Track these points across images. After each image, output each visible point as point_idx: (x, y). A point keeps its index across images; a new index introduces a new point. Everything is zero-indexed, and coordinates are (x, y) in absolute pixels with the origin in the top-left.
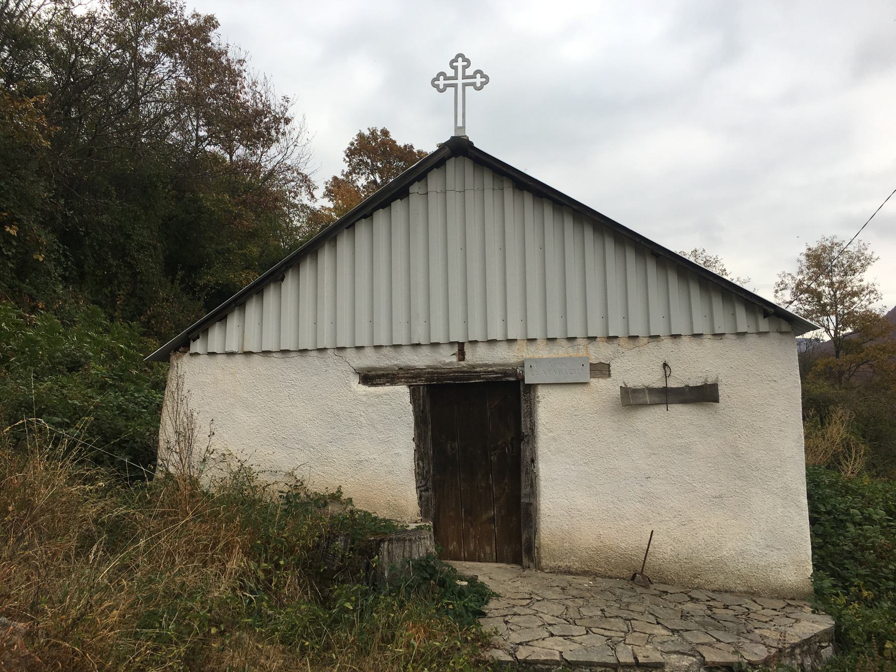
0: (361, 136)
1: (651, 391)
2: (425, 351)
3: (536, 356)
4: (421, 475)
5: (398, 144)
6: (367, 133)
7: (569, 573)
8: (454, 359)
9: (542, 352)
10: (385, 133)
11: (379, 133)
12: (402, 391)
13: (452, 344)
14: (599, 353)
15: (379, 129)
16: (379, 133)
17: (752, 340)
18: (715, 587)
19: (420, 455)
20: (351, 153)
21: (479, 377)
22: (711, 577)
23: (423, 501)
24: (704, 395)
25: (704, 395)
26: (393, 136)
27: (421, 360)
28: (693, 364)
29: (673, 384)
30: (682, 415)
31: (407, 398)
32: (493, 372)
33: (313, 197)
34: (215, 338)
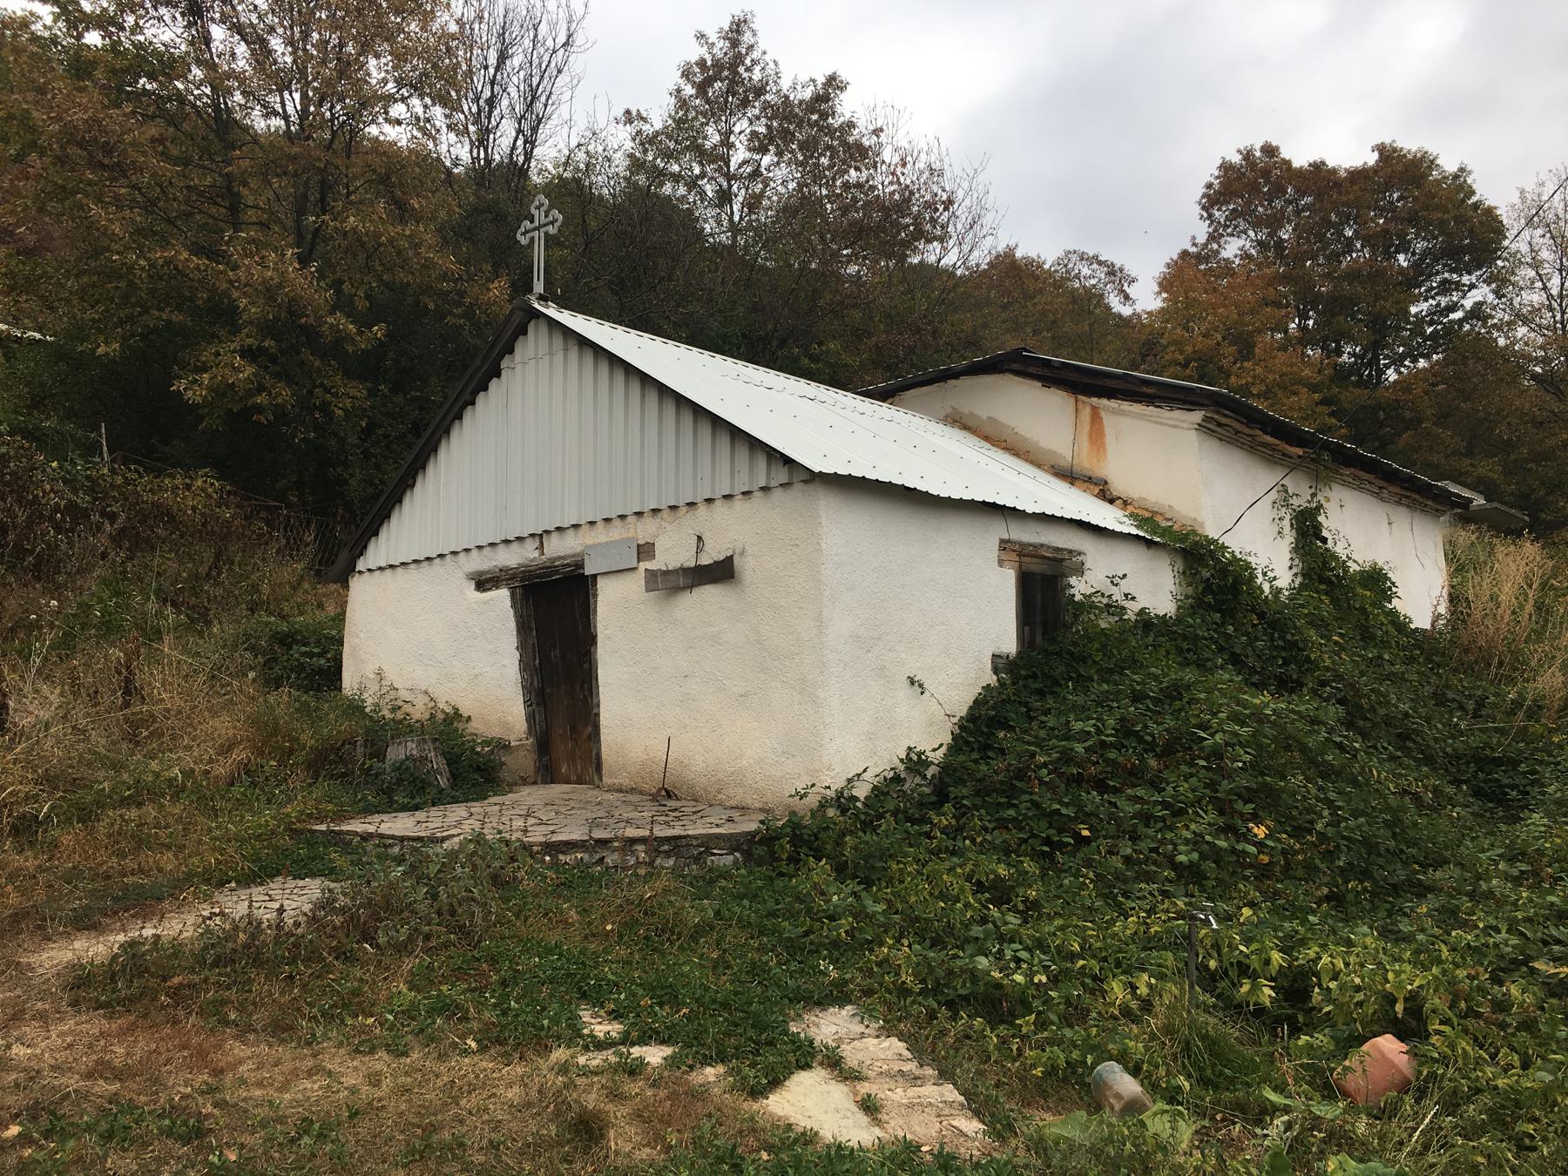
0: (1226, 167)
1: (685, 571)
2: (515, 546)
3: (597, 541)
4: (527, 688)
5: (1296, 164)
6: (1236, 159)
7: (621, 791)
8: (536, 554)
9: (600, 536)
10: (1270, 150)
11: (1258, 154)
12: (502, 595)
13: (532, 535)
14: (643, 531)
15: (1258, 146)
16: (1258, 154)
17: (778, 494)
18: (733, 803)
19: (525, 665)
20: (1212, 200)
21: (557, 572)
22: (731, 792)
23: (530, 718)
24: (722, 572)
25: (722, 572)
26: (1285, 154)
27: (511, 558)
28: (726, 531)
29: (706, 560)
30: (710, 594)
31: (508, 603)
32: (568, 565)
33: (1127, 297)
34: (378, 552)
